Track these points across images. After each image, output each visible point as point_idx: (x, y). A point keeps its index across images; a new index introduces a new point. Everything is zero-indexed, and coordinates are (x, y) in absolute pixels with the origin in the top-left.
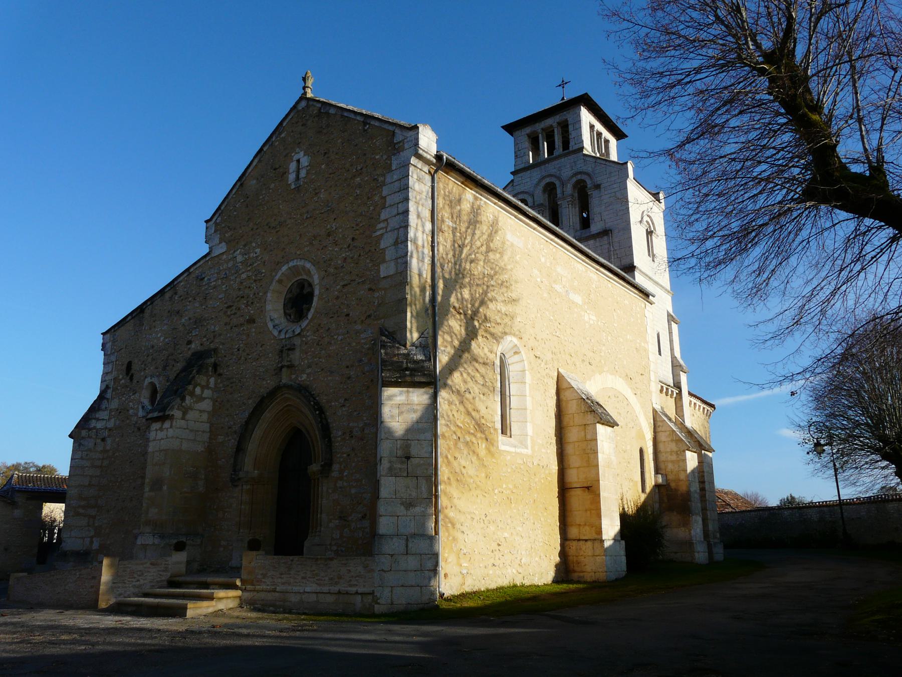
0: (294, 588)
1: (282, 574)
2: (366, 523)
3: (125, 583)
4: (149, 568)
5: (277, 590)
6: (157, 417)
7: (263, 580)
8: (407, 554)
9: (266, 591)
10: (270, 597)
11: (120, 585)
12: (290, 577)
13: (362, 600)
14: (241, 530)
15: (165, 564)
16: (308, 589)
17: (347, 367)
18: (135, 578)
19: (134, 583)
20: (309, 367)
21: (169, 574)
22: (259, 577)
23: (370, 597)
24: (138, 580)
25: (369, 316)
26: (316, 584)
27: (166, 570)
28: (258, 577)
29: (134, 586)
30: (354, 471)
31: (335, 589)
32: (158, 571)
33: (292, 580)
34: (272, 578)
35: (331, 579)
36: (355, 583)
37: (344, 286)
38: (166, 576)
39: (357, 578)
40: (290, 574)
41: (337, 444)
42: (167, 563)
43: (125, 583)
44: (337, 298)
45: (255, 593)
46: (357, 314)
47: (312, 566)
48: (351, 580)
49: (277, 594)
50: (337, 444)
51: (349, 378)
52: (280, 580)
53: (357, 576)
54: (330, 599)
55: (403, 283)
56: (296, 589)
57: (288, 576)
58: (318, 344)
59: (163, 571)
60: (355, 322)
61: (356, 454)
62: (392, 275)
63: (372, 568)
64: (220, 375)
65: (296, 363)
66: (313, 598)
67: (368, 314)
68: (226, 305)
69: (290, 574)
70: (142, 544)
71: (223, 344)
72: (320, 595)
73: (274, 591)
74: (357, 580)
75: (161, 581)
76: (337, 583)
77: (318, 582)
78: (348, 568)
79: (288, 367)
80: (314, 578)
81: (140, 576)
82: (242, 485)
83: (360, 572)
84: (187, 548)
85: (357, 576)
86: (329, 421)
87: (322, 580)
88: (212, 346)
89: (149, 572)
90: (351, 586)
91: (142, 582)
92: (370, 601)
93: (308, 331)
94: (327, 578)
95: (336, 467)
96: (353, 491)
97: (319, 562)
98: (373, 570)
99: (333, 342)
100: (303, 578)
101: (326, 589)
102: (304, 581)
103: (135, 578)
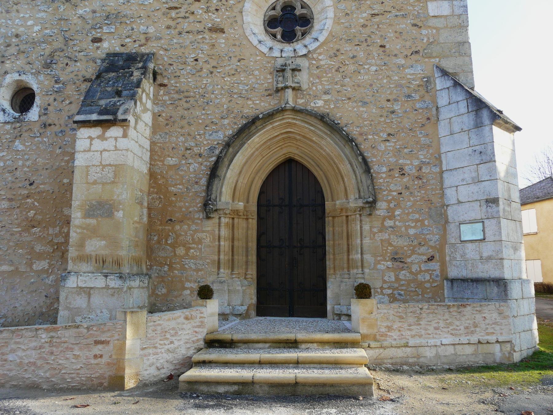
0: (429, 341)
1: (410, 325)
2: (435, 266)
3: (156, 348)
4: (184, 324)
5: (410, 345)
6: (94, 121)
7: (389, 334)
8: (523, 298)
9: (396, 347)
10: (400, 353)
11: (151, 351)
12: (421, 329)
13: (501, 349)
14: (222, 270)
15: (201, 317)
16: (445, 341)
17: (388, 100)
18: (167, 339)
19: (167, 347)
20: (326, 93)
21: (205, 331)
22: (383, 330)
23: (508, 345)
24: (172, 342)
25: (417, 52)
26: (452, 334)
27: (202, 325)
28: (381, 330)
29: (168, 350)
30: (411, 210)
31: (474, 339)
32: (194, 327)
33: (423, 332)
34: (399, 331)
35: (467, 328)
36: (492, 331)
37: (373, 15)
38: (202, 334)
39: (493, 326)
40: (420, 324)
41: (381, 181)
42: (202, 315)
43: (156, 348)
44: (365, 26)
45: (382, 350)
46: (398, 47)
47: (444, 315)
48: (487, 328)
49: (408, 350)
50: (381, 181)
51: (393, 112)
52: (409, 333)
53: (493, 324)
54: (469, 350)
55: (463, 26)
56: (432, 342)
57: (418, 327)
58: (337, 70)
59: (199, 327)
60: (396, 55)
61: (411, 193)
62: (447, 16)
63: (507, 314)
64: (161, 85)
65: (305, 86)
66: (450, 350)
67: (414, 49)
68: (167, 6)
69: (420, 324)
70: (78, 287)
71: (166, 50)
72: (457, 347)
73: (406, 346)
74: (493, 328)
75: (198, 340)
76: (472, 333)
77: (453, 332)
78: (484, 315)
79: (294, 89)
80: (448, 328)
81: (173, 336)
82: (220, 218)
83: (496, 319)
84: (215, 295)
85: (493, 324)
86: (365, 154)
87: (457, 330)
88: (144, 50)
89: (182, 329)
90: (488, 334)
91: (176, 343)
92: (509, 349)
93: (320, 54)
94: (462, 328)
95: (382, 205)
96: (412, 232)
97: (451, 310)
98: (508, 316)
99: (362, 71)
100: (436, 328)
101: (464, 340)
102: (437, 331)
103: (167, 339)
